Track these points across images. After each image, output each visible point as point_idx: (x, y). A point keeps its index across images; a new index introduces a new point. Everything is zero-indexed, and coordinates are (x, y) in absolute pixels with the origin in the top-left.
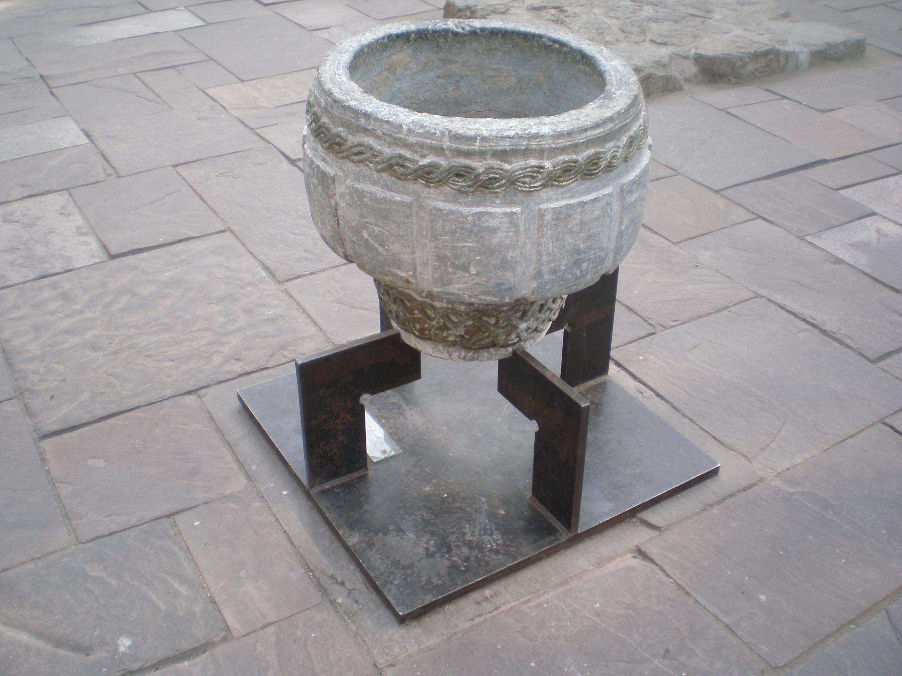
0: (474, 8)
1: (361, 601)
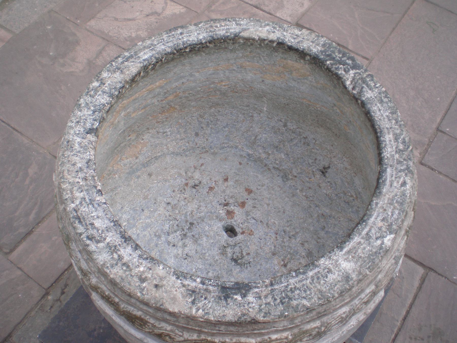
0: (313, 62)
1: (53, 310)
